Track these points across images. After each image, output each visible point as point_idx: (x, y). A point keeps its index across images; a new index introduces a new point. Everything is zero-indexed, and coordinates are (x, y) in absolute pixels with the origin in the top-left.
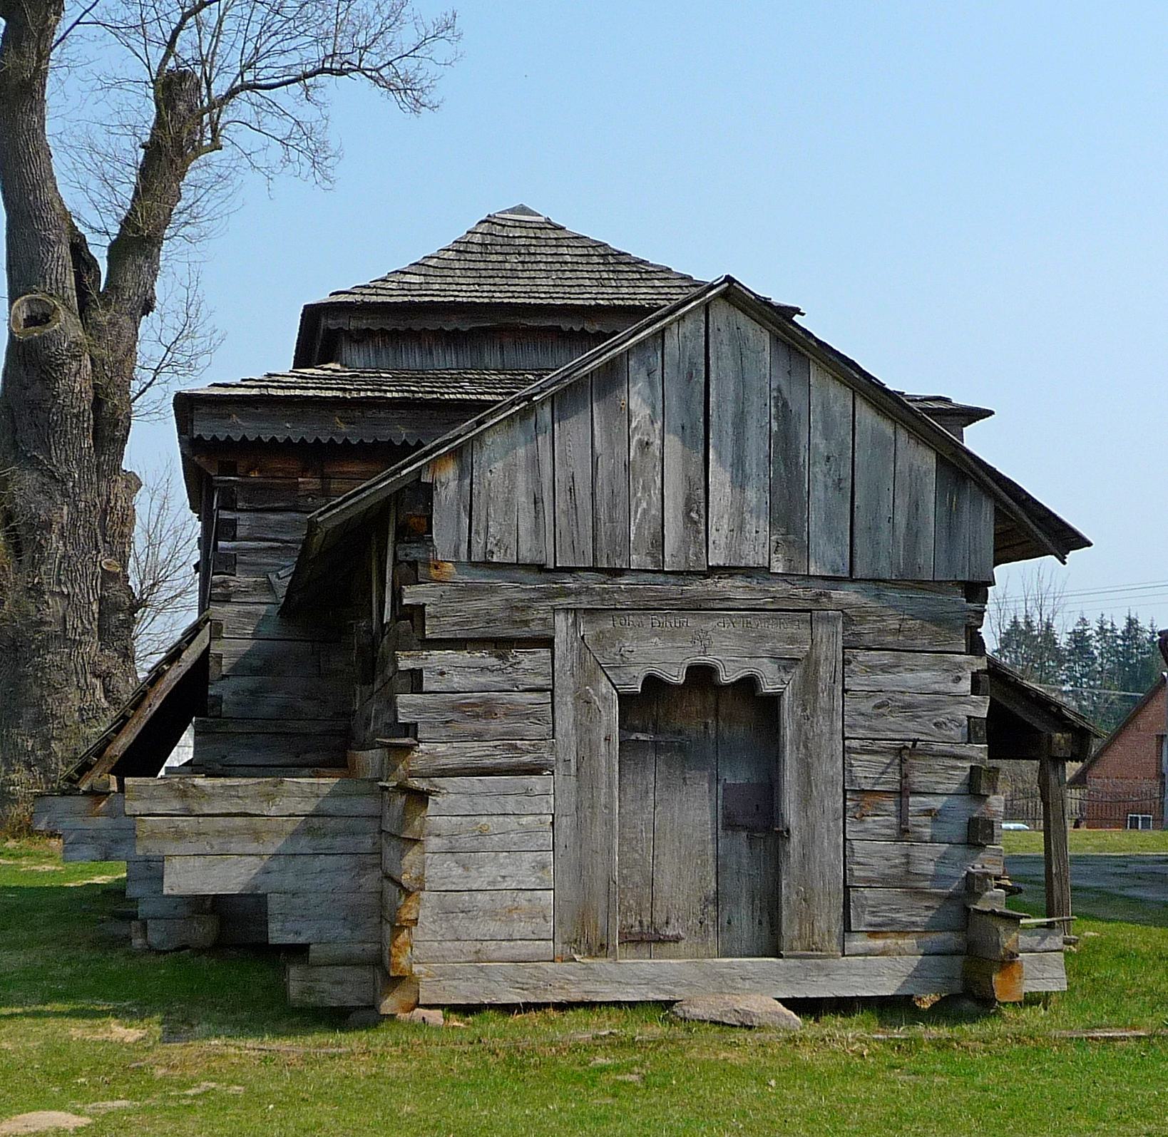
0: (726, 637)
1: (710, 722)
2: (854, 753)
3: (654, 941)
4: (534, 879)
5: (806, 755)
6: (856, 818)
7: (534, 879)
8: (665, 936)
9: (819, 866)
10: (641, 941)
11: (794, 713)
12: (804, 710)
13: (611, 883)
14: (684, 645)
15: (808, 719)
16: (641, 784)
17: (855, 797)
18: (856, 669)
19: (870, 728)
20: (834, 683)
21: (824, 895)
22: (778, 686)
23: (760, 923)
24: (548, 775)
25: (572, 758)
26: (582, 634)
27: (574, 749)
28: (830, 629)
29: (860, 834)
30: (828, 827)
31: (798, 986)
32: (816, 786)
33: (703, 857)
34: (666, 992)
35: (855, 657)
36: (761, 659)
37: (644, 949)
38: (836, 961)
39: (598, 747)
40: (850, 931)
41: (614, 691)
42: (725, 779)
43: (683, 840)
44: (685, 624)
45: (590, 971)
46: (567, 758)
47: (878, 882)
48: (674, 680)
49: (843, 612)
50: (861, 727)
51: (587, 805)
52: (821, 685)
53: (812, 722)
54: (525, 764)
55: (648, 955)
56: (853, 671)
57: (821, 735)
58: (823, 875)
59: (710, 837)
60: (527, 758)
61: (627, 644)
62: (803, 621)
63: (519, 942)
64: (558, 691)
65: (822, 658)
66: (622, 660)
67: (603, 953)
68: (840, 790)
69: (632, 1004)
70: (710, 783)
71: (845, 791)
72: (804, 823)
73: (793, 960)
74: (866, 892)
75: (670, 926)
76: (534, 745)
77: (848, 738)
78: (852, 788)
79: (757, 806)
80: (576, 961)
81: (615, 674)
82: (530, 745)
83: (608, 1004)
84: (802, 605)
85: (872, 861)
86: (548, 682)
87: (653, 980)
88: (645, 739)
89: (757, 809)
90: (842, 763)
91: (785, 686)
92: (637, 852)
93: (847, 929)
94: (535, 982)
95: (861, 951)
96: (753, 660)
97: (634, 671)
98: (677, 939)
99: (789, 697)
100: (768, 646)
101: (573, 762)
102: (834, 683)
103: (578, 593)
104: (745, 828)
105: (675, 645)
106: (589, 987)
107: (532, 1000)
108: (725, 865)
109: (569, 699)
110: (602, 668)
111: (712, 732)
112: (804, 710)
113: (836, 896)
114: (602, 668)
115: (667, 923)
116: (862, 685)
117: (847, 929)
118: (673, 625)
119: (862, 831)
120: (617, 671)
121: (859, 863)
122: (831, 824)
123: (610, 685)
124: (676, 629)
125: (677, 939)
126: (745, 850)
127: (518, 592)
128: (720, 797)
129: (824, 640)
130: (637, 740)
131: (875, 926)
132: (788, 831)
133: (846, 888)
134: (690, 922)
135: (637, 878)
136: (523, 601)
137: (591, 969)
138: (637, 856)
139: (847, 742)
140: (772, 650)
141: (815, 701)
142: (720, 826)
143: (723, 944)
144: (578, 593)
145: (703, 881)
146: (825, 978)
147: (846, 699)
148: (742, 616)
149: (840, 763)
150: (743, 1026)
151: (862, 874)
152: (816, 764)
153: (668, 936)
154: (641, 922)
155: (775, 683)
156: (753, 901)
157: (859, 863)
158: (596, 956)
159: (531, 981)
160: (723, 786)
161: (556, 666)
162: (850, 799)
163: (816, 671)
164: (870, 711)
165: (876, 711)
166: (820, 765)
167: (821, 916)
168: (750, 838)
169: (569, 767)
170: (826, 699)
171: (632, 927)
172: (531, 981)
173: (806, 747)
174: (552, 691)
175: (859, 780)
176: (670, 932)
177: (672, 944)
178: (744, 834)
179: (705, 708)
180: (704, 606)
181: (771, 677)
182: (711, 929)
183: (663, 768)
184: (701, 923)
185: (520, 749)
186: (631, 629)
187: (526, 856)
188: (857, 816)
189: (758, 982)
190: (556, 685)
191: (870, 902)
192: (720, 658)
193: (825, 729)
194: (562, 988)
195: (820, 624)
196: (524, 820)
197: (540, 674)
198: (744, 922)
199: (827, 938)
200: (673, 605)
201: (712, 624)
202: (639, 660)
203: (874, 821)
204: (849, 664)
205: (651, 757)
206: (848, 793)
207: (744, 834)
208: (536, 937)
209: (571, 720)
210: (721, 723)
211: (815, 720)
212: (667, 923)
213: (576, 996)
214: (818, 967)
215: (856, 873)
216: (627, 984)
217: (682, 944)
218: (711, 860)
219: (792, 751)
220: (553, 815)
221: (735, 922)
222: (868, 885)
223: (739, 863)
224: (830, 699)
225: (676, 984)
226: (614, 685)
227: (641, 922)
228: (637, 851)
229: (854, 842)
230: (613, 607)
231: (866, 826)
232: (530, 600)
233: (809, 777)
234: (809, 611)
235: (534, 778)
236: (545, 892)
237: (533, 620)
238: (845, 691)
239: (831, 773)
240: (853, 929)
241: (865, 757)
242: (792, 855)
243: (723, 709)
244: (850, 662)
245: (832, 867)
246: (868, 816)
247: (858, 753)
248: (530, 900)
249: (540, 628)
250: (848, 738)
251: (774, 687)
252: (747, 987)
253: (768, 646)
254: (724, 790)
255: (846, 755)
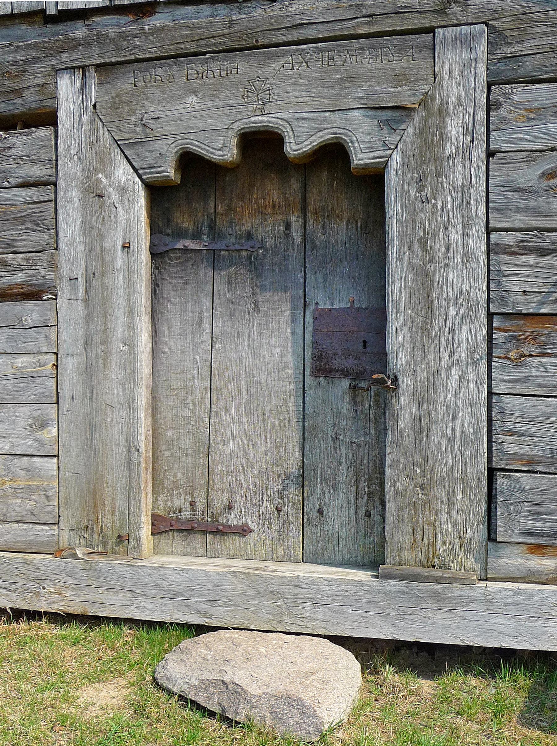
0: (294, 84)
1: (294, 219)
2: (503, 254)
3: (211, 532)
4: (31, 442)
5: (423, 259)
6: (509, 359)
7: (31, 442)
8: (225, 526)
9: (446, 435)
10: (192, 531)
11: (405, 193)
12: (421, 188)
13: (133, 450)
14: (232, 102)
15: (428, 202)
16: (193, 311)
17: (506, 324)
18: (510, 116)
19: (535, 212)
20: (472, 141)
21: (454, 480)
22: (379, 153)
23: (368, 514)
24: (49, 299)
25: (80, 277)
26: (94, 101)
27: (83, 262)
28: (465, 54)
29: (515, 385)
30: (462, 374)
31: (402, 624)
32: (441, 308)
33: (283, 416)
34: (200, 613)
35: (507, 96)
36: (349, 114)
37: (197, 541)
38: (467, 588)
39: (113, 259)
40: (494, 540)
41: (137, 179)
42: (317, 303)
43: (253, 391)
44: (234, 71)
45: (95, 573)
46: (73, 276)
47: (544, 464)
48: (216, 156)
49: (487, 25)
50: (519, 210)
51: (99, 340)
52: (449, 147)
53: (435, 205)
54: (20, 285)
55: (201, 551)
56: (504, 119)
57: (447, 227)
58: (451, 450)
59: (292, 387)
60: (19, 278)
61: (152, 109)
62: (421, 48)
63: (15, 525)
64: (61, 183)
65: (452, 101)
66: (144, 131)
67: (120, 549)
68: (482, 315)
69: (151, 625)
70: (294, 309)
71: (490, 316)
72: (420, 368)
73: (395, 582)
74: (524, 479)
75: (234, 512)
76: (28, 260)
77: (496, 230)
78: (502, 311)
79: (365, 342)
80: (78, 558)
81: (137, 154)
82: (23, 259)
83: (117, 621)
84: (417, 22)
85: (535, 430)
86: (49, 172)
87: (178, 594)
88: (197, 247)
89: (365, 346)
90: (484, 269)
91: (389, 152)
92: (186, 406)
93: (491, 537)
94: (25, 582)
95: (515, 573)
96: (337, 115)
97: (161, 146)
98: (244, 531)
99: (397, 170)
100: (362, 91)
101: (81, 281)
102: (472, 141)
103: (86, 44)
104: (345, 373)
105: (219, 103)
106: (92, 596)
107: (23, 605)
108: (314, 428)
109: (75, 193)
110: (118, 145)
111: (296, 234)
112: (421, 188)
113: (474, 484)
114: (118, 145)
115: (230, 508)
116: (520, 141)
117: (491, 537)
118: (217, 74)
119: (518, 381)
120: (139, 150)
121: (513, 433)
122: (467, 370)
123: (131, 170)
124: (220, 79)
125: (244, 531)
126: (346, 407)
127: (11, 52)
128: (309, 330)
129: (455, 74)
130: (186, 250)
131: (538, 535)
132: (395, 380)
133: (492, 472)
134: (263, 509)
135: (187, 443)
136: (15, 63)
137: (95, 570)
138: (186, 412)
139: (494, 237)
140: (368, 96)
141: (440, 174)
142: (308, 372)
143: (311, 543)
144: (86, 44)
145: (282, 450)
146: (448, 615)
147: (491, 166)
148: (321, 50)
149: (482, 270)
150: (224, 718)
151: (519, 450)
152: (441, 272)
153: (230, 526)
154: (192, 504)
155: (372, 149)
156: (358, 481)
157: (513, 433)
158: (114, 552)
159: (19, 580)
160: (313, 312)
161: (60, 150)
162: (498, 329)
163: (442, 125)
164: (534, 183)
165: (546, 183)
166: (448, 273)
167: (448, 513)
168: (354, 389)
169: (74, 289)
170: (458, 169)
171: (180, 511)
172: (19, 580)
173: (424, 246)
174: (55, 184)
175: (513, 298)
176: (233, 520)
177: (236, 538)
178: (345, 383)
179: (286, 199)
180: (261, 41)
181: (367, 139)
182: (292, 519)
183: (220, 284)
184: (279, 510)
185: (10, 265)
186: (158, 86)
187: (21, 409)
188: (512, 355)
189: (337, 612)
190: (60, 174)
191: (530, 497)
192: (286, 116)
193: (457, 217)
194: (57, 593)
195: (448, 51)
196: (20, 362)
197: (38, 161)
198: (344, 513)
199: (457, 548)
200: (216, 44)
201: (274, 66)
202: (169, 129)
203: (543, 365)
204: (498, 108)
205: (206, 273)
206: (495, 319)
207: (345, 383)
208: (34, 519)
209: (79, 223)
210: (311, 221)
211: (440, 205)
212: (230, 508)
213: (75, 608)
214: (436, 596)
215: (509, 449)
216: (144, 596)
217: (251, 538)
218: (294, 421)
219: (400, 254)
220: (56, 354)
221: (329, 512)
222: (530, 468)
223: (337, 426)
224: (464, 167)
225: (213, 602)
226: (136, 170)
227: (192, 504)
228: (186, 406)
229: (506, 399)
230: (132, 57)
231: (527, 372)
232: (27, 61)
233: (429, 293)
234: (431, 30)
235: (30, 305)
236: (46, 459)
237: (27, 88)
238: (490, 154)
239: (466, 287)
240: (499, 538)
241: (525, 260)
242: (401, 416)
243: (314, 200)
244: (498, 105)
245: (468, 436)
246: (531, 356)
247: (512, 253)
248: (27, 470)
249: (37, 97)
250: (496, 230)
251: (371, 155)
252: (321, 617)
253: (362, 91)
254: (315, 318)
255: (492, 257)
